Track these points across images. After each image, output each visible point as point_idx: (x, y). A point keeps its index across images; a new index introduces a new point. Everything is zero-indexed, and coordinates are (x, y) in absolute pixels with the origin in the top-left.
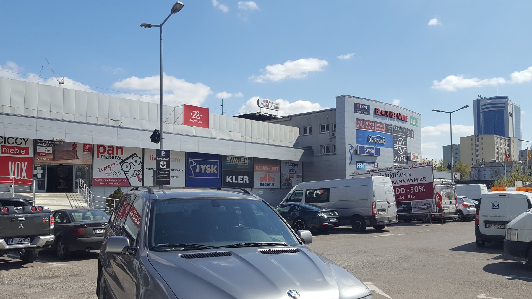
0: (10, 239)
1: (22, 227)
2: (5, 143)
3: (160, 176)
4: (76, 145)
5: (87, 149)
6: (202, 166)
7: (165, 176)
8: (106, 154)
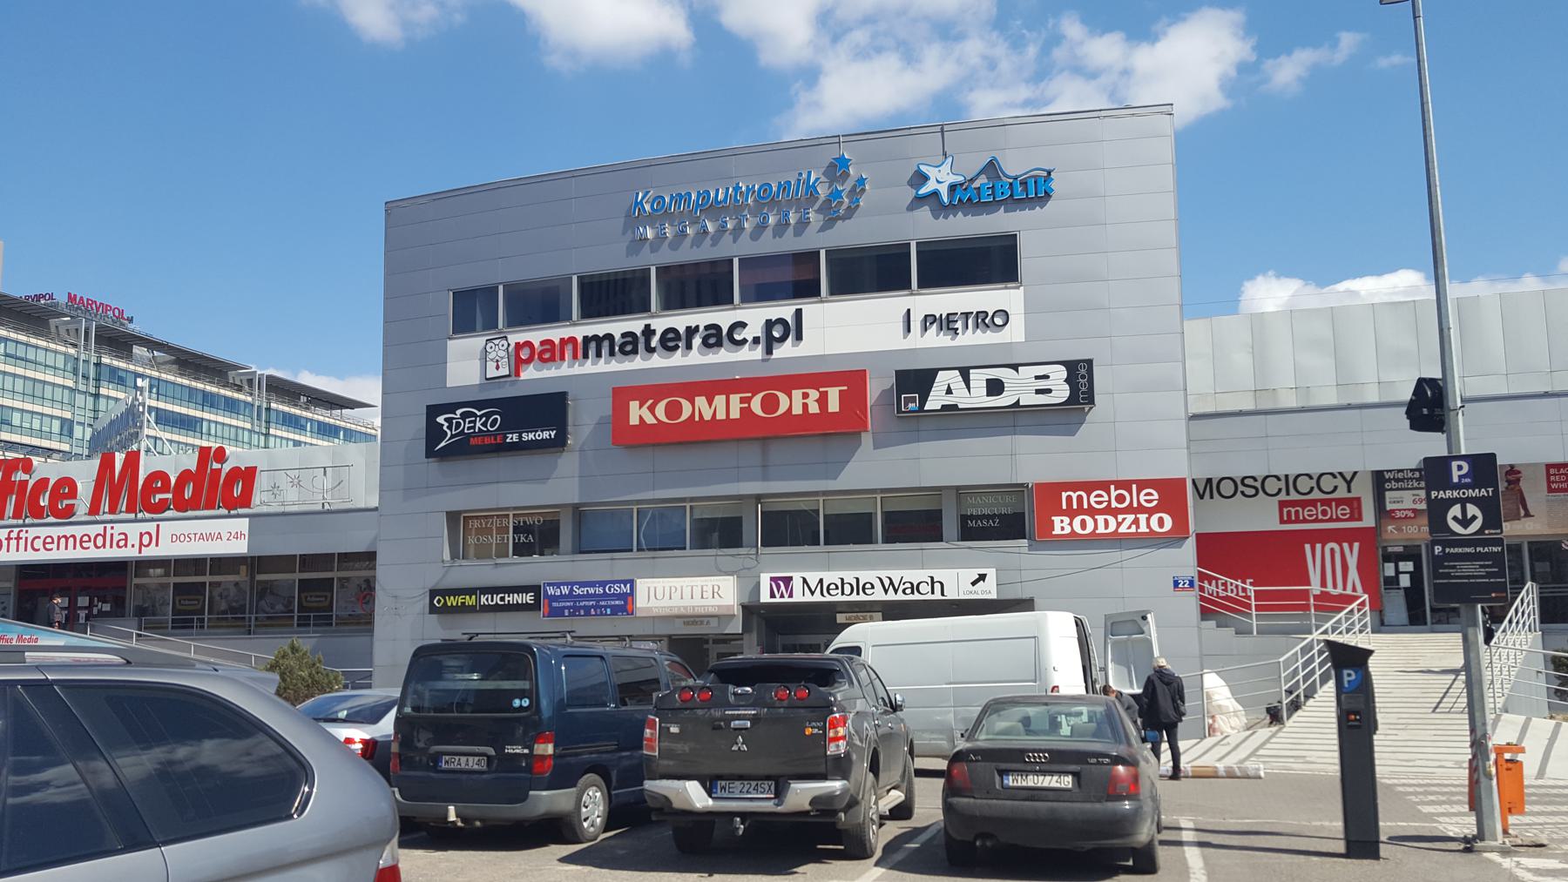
0: (719, 782)
1: (742, 749)
2: (1288, 494)
3: (1454, 567)
4: (1519, 472)
5: (1562, 482)
7: (1481, 566)
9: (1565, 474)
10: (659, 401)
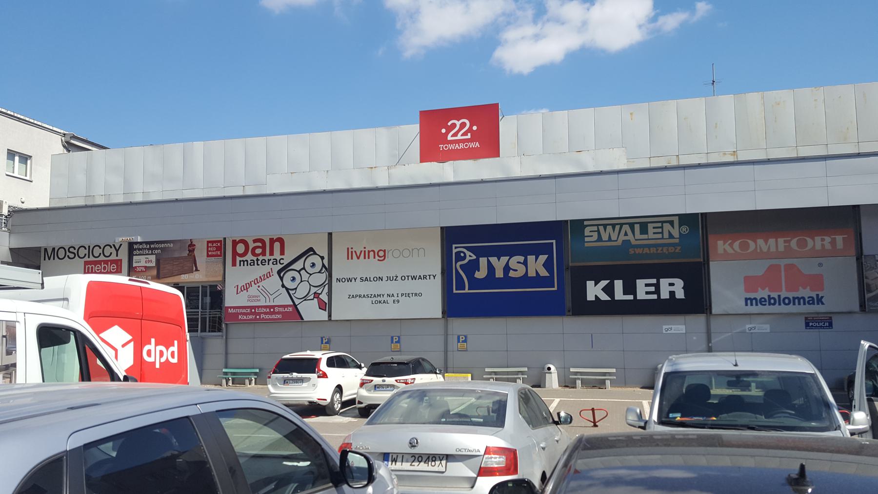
2: (89, 257)
4: (195, 245)
5: (213, 251)
6: (494, 260)
8: (249, 257)
9: (215, 247)
10: (735, 242)
